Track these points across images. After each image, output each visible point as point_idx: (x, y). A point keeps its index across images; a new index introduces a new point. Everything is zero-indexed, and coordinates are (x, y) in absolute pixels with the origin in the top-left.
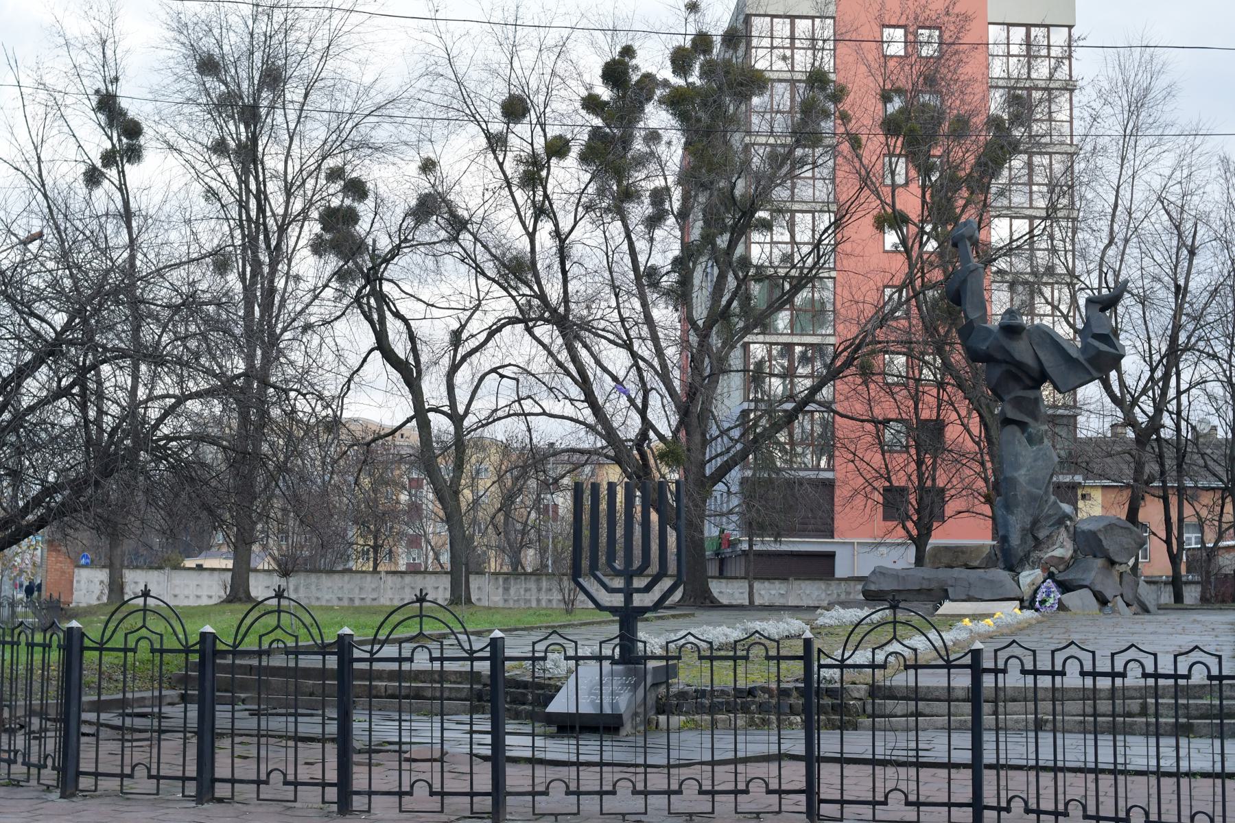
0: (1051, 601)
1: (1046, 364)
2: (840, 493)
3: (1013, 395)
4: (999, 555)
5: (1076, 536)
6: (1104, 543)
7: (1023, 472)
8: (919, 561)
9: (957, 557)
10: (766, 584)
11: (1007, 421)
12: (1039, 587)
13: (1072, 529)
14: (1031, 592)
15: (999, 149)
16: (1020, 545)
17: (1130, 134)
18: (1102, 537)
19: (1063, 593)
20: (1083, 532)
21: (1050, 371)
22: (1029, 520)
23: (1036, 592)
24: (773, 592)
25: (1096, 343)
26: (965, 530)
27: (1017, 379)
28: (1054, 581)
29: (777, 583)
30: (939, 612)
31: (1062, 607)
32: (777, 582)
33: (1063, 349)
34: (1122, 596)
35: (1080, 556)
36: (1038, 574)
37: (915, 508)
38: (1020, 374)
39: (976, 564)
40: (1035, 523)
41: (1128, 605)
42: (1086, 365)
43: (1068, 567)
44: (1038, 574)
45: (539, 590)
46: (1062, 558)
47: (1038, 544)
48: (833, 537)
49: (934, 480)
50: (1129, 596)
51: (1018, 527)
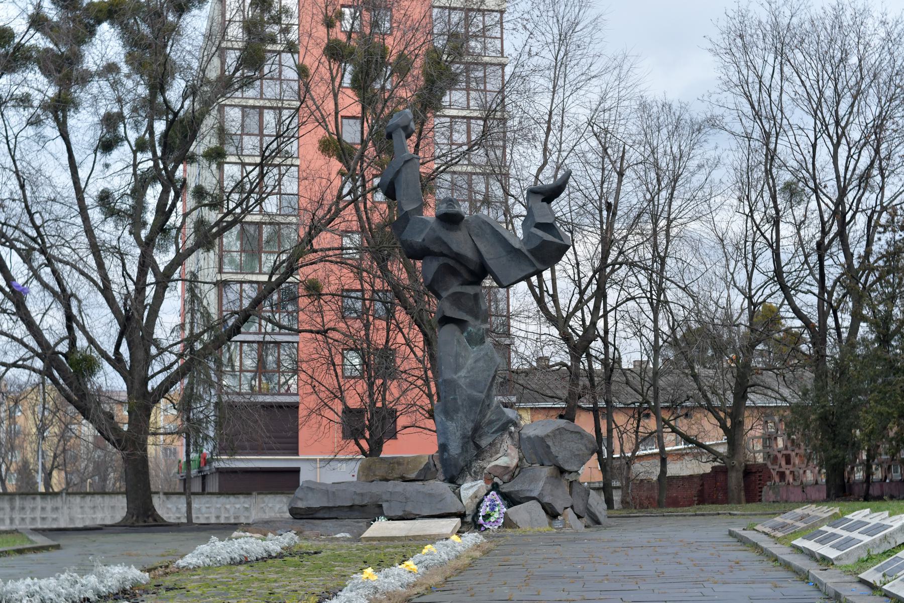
0: (496, 515)
1: (486, 256)
2: (302, 412)
3: (451, 291)
4: (439, 466)
5: (520, 443)
6: (553, 449)
7: (463, 373)
8: (367, 473)
9: (397, 471)
10: (232, 499)
11: (445, 320)
12: (482, 501)
13: (516, 436)
14: (474, 506)
15: (438, 79)
16: (460, 455)
17: (560, 65)
18: (550, 444)
19: (509, 507)
20: (529, 438)
21: (491, 263)
22: (470, 426)
23: (478, 506)
24: (238, 506)
25: (540, 233)
26: (414, 443)
27: (454, 273)
28: (499, 493)
29: (242, 498)
30: (368, 534)
31: (508, 523)
32: (241, 497)
33: (505, 239)
34: (572, 507)
35: (526, 465)
36: (480, 485)
37: (369, 427)
38: (458, 267)
39: (413, 476)
40: (477, 429)
41: (579, 517)
42: (529, 255)
43: (513, 477)
44: (480, 485)
45: (12, 509)
46: (507, 468)
47: (480, 453)
48: (297, 454)
49: (384, 399)
50: (580, 508)
51: (458, 434)
